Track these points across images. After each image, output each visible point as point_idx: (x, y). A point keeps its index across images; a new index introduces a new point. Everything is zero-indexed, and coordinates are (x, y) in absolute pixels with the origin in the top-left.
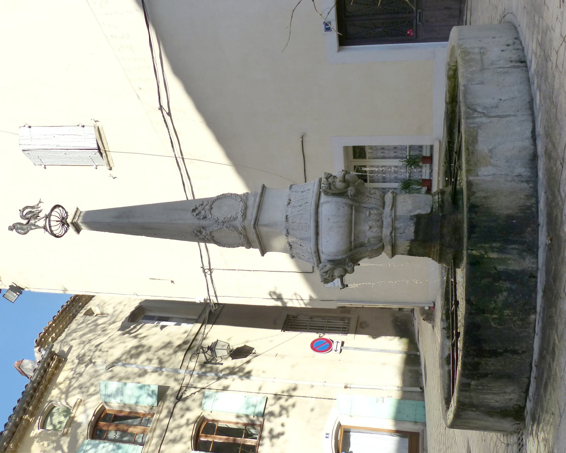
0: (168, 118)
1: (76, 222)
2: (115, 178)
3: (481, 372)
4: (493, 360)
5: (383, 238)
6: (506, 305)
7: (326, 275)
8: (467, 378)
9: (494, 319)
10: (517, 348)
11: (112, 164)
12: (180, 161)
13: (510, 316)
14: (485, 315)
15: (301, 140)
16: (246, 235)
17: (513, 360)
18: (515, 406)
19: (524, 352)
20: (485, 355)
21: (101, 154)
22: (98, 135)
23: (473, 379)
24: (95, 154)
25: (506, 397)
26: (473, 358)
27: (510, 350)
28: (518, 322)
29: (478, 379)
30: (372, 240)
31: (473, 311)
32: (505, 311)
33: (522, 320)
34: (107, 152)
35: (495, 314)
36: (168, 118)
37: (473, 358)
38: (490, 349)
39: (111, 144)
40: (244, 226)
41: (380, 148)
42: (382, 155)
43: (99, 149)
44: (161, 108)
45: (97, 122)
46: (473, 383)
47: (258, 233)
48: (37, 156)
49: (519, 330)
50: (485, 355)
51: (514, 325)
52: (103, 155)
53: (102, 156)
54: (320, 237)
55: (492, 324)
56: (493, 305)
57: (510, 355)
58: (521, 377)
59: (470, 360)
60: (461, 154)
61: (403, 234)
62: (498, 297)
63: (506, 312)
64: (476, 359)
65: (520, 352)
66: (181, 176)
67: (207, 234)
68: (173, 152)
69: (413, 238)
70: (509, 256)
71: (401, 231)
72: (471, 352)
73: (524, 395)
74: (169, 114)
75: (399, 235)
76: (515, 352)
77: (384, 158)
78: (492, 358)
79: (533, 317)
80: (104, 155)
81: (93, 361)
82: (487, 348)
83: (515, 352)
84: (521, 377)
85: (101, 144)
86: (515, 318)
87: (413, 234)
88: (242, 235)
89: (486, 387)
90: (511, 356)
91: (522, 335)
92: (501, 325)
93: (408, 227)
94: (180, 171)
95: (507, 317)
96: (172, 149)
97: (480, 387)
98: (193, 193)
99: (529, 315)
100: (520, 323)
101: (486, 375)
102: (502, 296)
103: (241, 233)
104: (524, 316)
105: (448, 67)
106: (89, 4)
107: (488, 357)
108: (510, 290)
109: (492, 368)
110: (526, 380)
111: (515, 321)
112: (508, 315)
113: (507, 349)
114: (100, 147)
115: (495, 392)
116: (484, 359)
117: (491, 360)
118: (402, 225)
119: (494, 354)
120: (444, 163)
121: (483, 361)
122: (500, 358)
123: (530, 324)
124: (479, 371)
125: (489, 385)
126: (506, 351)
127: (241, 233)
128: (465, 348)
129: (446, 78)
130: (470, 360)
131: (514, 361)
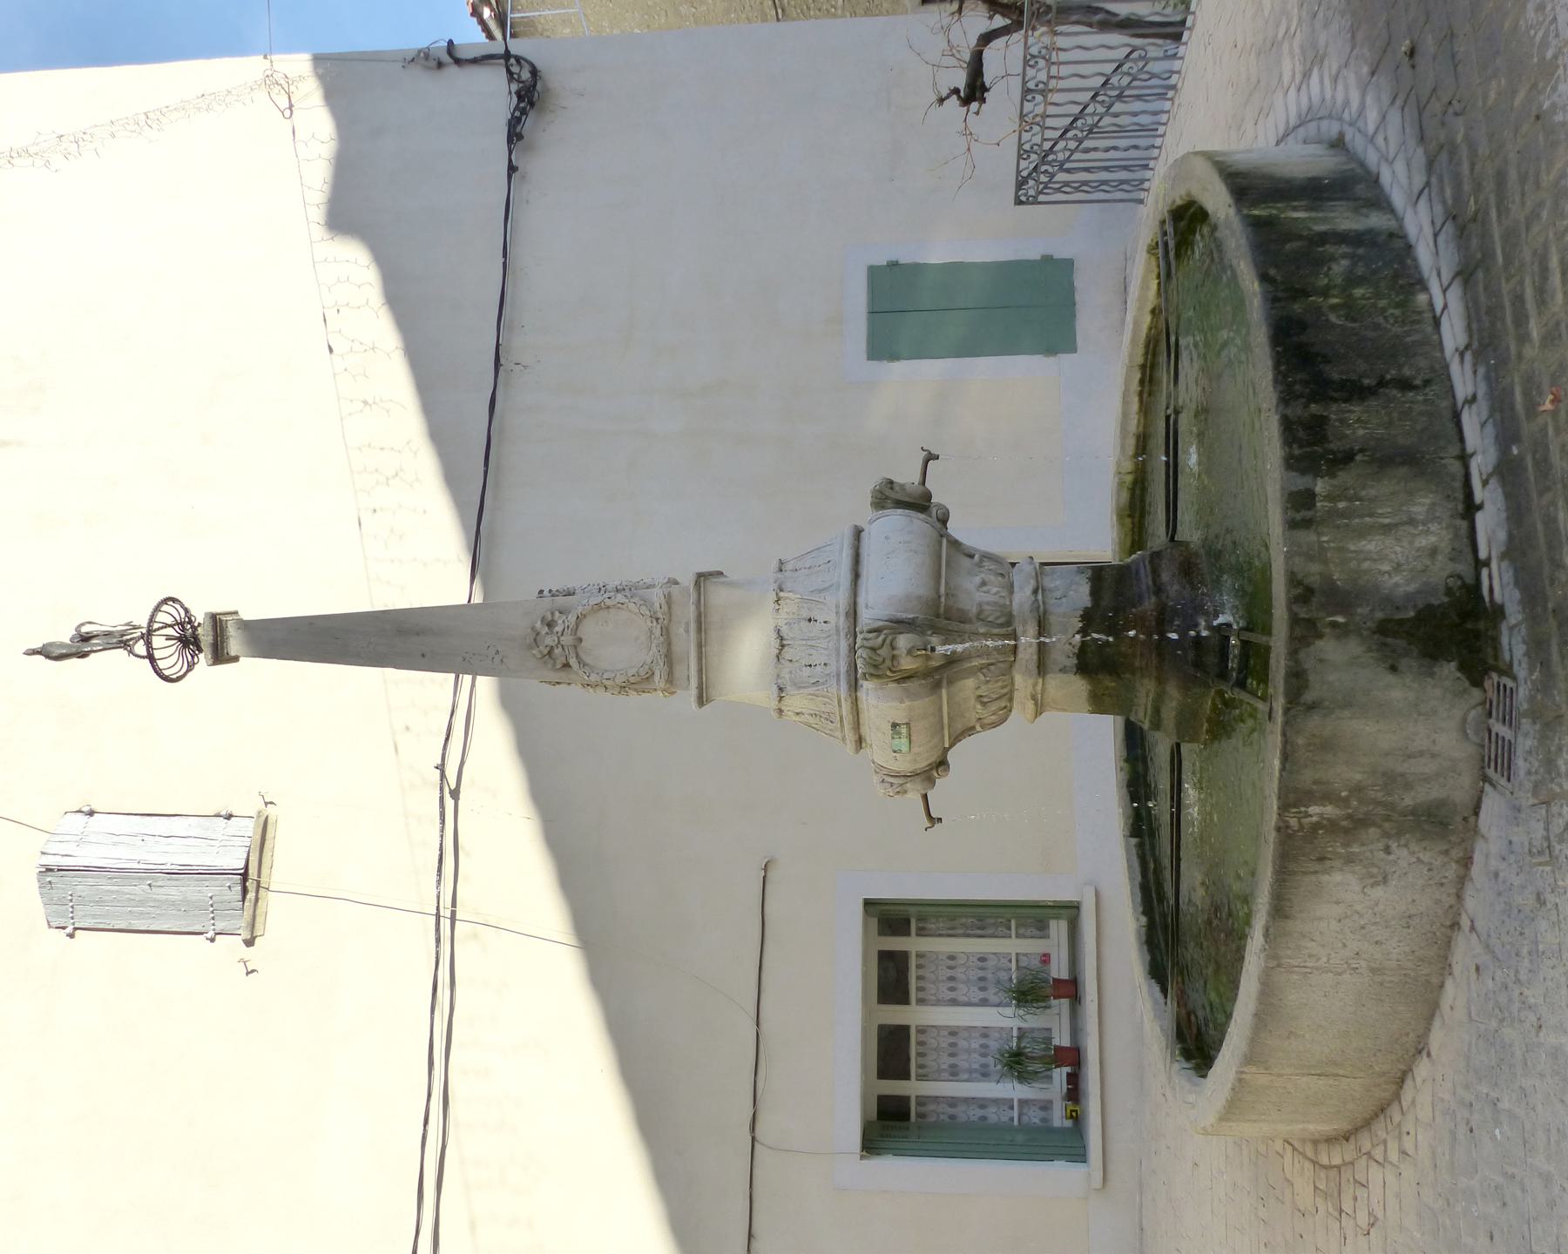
0: (449, 803)
1: (224, 623)
2: (253, 971)
3: (1332, 446)
4: (1356, 410)
5: (1015, 613)
6: (1352, 280)
7: (877, 637)
8: (1303, 472)
9: (1333, 308)
10: (1407, 372)
11: (262, 927)
12: (445, 924)
13: (1369, 298)
14: (1311, 299)
15: (763, 874)
16: (667, 629)
17: (1407, 405)
18: (1451, 581)
19: (1427, 383)
20: (1335, 395)
21: (245, 891)
22: (258, 837)
23: (1317, 474)
24: (229, 887)
25: (1417, 544)
26: (1306, 406)
27: (1391, 380)
28: (1391, 311)
29: (1333, 475)
30: (986, 607)
31: (1280, 294)
32: (1355, 291)
33: (1398, 305)
34: (262, 891)
35: (1334, 296)
36: (449, 803)
37: (1306, 406)
38: (1342, 379)
39: (281, 871)
40: (669, 593)
41: (945, 978)
42: (952, 995)
43: (245, 876)
44: (441, 768)
45: (269, 805)
46: (1321, 486)
47: (702, 609)
48: (70, 893)
49: (1399, 329)
50: (1335, 395)
51: (1386, 318)
52: (248, 897)
53: (243, 900)
54: (863, 581)
55: (1333, 318)
56: (1323, 281)
57: (1395, 393)
58: (1442, 458)
59: (1296, 411)
60: (1145, 947)
61: (1064, 600)
62: (1329, 269)
63: (1358, 292)
64: (1314, 408)
65: (1418, 382)
66: (434, 959)
67: (568, 627)
68: (434, 884)
69: (1089, 605)
70: (1332, 215)
71: (1058, 594)
72: (1297, 387)
73: (1464, 524)
74: (455, 794)
75: (1054, 601)
76: (1405, 385)
77: (954, 1002)
78: (1354, 403)
79: (1422, 298)
80: (251, 895)
81: (196, 624)
82: (1336, 376)
83: (1405, 385)
84: (1442, 458)
85: (256, 863)
86: (1382, 303)
87: (1089, 598)
88: (659, 626)
89: (1358, 503)
90: (1399, 395)
91: (1408, 339)
92: (1354, 320)
93: (1074, 587)
94: (437, 947)
95: (1364, 302)
96: (434, 877)
97: (1341, 505)
98: (451, 1029)
99: (1413, 294)
100: (1397, 312)
101: (1347, 458)
102: (1339, 268)
103: (657, 619)
104: (1402, 297)
105: (1117, 479)
106: (361, 536)
107: (1345, 401)
108: (1352, 256)
109: (1361, 432)
110: (1455, 467)
111: (1383, 310)
112: (1363, 297)
113: (1382, 377)
114: (250, 871)
115: (1387, 521)
116: (1334, 407)
117: (1352, 408)
118: (1058, 583)
119: (1355, 391)
120: (1122, 764)
121: (1333, 412)
122: (1373, 402)
123: (1420, 313)
124: (1326, 445)
125: (1363, 493)
126: (1382, 383)
127: (657, 619)
128: (1280, 378)
129: (1115, 518)
130: (1296, 411)
131: (1410, 408)
